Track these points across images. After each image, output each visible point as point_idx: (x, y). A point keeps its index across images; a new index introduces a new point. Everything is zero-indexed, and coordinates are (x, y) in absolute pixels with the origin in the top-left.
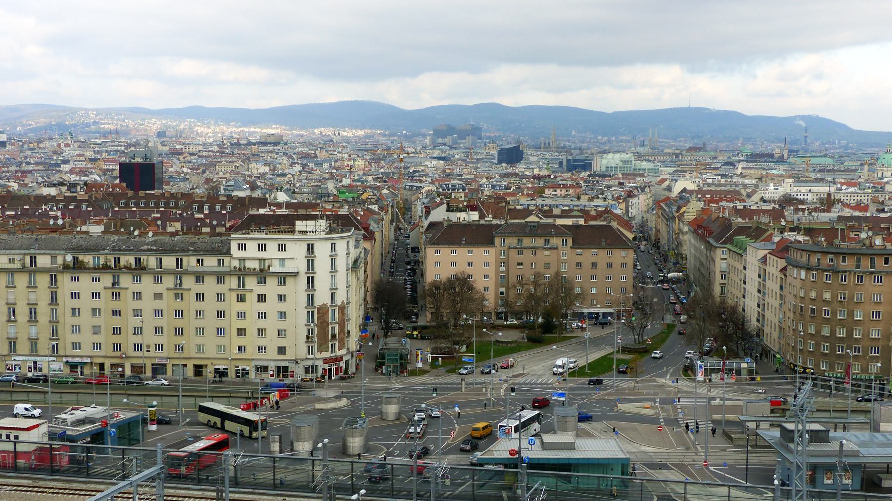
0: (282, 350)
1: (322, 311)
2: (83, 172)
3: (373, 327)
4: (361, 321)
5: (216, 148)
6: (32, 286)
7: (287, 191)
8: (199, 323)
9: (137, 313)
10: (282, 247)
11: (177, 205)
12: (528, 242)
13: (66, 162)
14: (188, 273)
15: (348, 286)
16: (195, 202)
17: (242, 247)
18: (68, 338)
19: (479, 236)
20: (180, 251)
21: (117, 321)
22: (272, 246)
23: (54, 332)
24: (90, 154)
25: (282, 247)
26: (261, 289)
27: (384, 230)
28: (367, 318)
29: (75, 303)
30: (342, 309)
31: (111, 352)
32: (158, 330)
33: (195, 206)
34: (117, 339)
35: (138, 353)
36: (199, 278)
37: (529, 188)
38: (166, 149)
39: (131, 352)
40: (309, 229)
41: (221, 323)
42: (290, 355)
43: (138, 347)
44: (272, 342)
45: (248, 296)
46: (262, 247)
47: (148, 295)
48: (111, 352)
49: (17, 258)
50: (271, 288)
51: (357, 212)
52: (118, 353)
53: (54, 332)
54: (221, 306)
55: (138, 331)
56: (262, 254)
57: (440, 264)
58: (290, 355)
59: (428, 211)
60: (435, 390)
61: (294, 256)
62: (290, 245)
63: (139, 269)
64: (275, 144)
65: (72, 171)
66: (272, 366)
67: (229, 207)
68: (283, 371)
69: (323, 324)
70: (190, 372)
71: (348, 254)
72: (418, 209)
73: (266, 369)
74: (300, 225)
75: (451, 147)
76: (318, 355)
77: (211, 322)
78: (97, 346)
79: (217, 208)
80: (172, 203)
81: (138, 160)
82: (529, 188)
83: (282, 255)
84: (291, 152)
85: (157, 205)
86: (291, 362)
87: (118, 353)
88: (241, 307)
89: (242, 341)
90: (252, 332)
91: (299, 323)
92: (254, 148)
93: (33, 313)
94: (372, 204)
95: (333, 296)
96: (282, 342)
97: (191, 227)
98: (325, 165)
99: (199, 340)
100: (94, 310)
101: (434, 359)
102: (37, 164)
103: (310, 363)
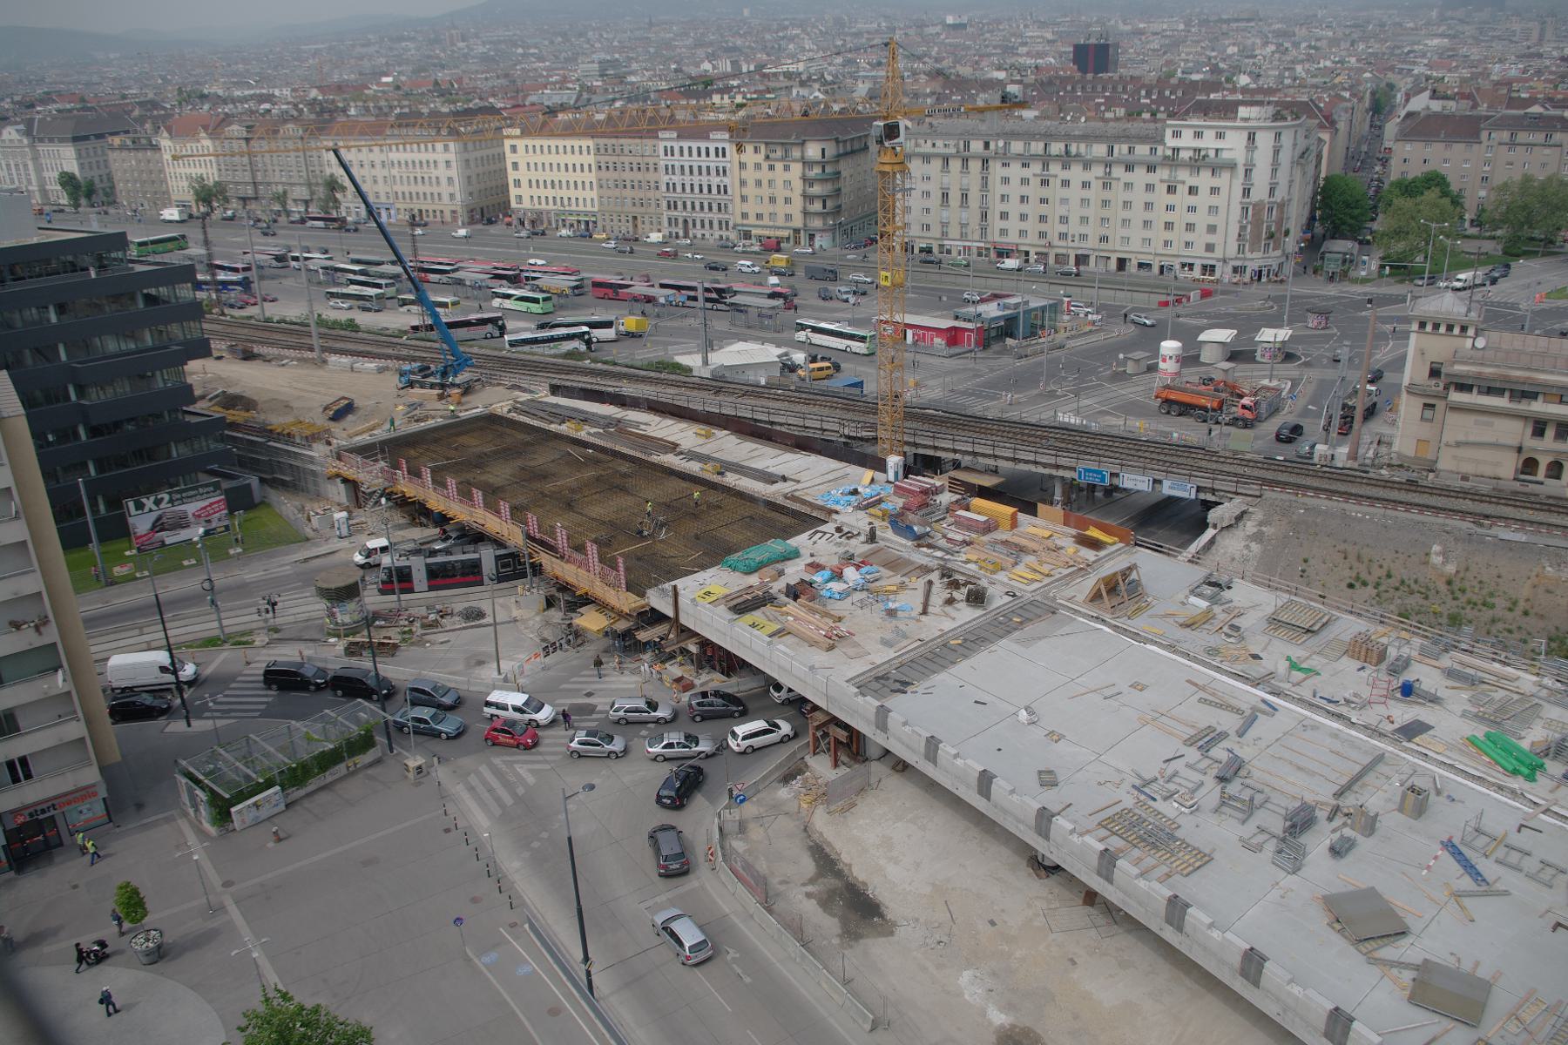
0: (1210, 248)
1: (1258, 206)
2: (1040, 55)
3: (1318, 229)
4: (1304, 220)
5: (1182, 27)
6: (787, 168)
7: (1250, 74)
8: (1126, 214)
9: (1064, 201)
10: (1220, 136)
11: (1124, 88)
12: (1522, 137)
13: (1025, 44)
14: (1119, 162)
15: (1291, 181)
16: (1143, 86)
17: (1177, 134)
18: (996, 224)
19: (1466, 129)
20: (1111, 140)
21: (1044, 209)
22: (1209, 135)
23: (984, 216)
24: (1049, 36)
25: (1220, 136)
26: (1065, 175)
27: (1351, 119)
28: (1312, 218)
29: (1004, 190)
30: (1281, 206)
31: (1036, 241)
32: (1084, 220)
33: (1143, 93)
34: (1043, 227)
35: (1063, 243)
36: (1129, 167)
37: (1551, 73)
38: (1128, 28)
39: (1056, 242)
40: (1253, 115)
41: (1148, 216)
42: (1218, 253)
43: (1063, 236)
44: (1200, 238)
45: (1179, 187)
46: (1198, 135)
47: (1076, 184)
48: (1036, 241)
49: (952, 143)
50: (1204, 180)
51: (1320, 99)
52: (1043, 242)
53: (984, 216)
54: (1149, 197)
55: (1064, 220)
56: (1198, 144)
57: (1409, 158)
58: (1218, 253)
59: (1408, 98)
60: (1370, 301)
61: (1233, 145)
62: (1229, 134)
63: (1067, 159)
64: (1249, 20)
65: (1028, 54)
66: (1198, 264)
67: (1180, 93)
68: (1208, 269)
69: (1257, 223)
70: (1113, 265)
71: (1295, 145)
72: (1399, 97)
73: (1191, 266)
74: (1243, 111)
75: (1462, 21)
76: (1248, 255)
77: (1137, 214)
78: (1022, 233)
79: (1167, 93)
80: (1120, 89)
81: (1093, 41)
82: (1551, 73)
83: (1220, 144)
84: (1266, 29)
85: (1104, 89)
86: (1218, 260)
87: (1043, 242)
88: (1170, 199)
89: (1168, 235)
90: (1180, 226)
91: (1231, 220)
92: (1225, 26)
93: (964, 196)
94: (1345, 89)
95: (1272, 191)
96: (1211, 239)
97: (1133, 114)
98: (1304, 45)
99: (1124, 232)
100: (1022, 197)
101: (1382, 267)
102: (995, 47)
103: (1239, 263)
